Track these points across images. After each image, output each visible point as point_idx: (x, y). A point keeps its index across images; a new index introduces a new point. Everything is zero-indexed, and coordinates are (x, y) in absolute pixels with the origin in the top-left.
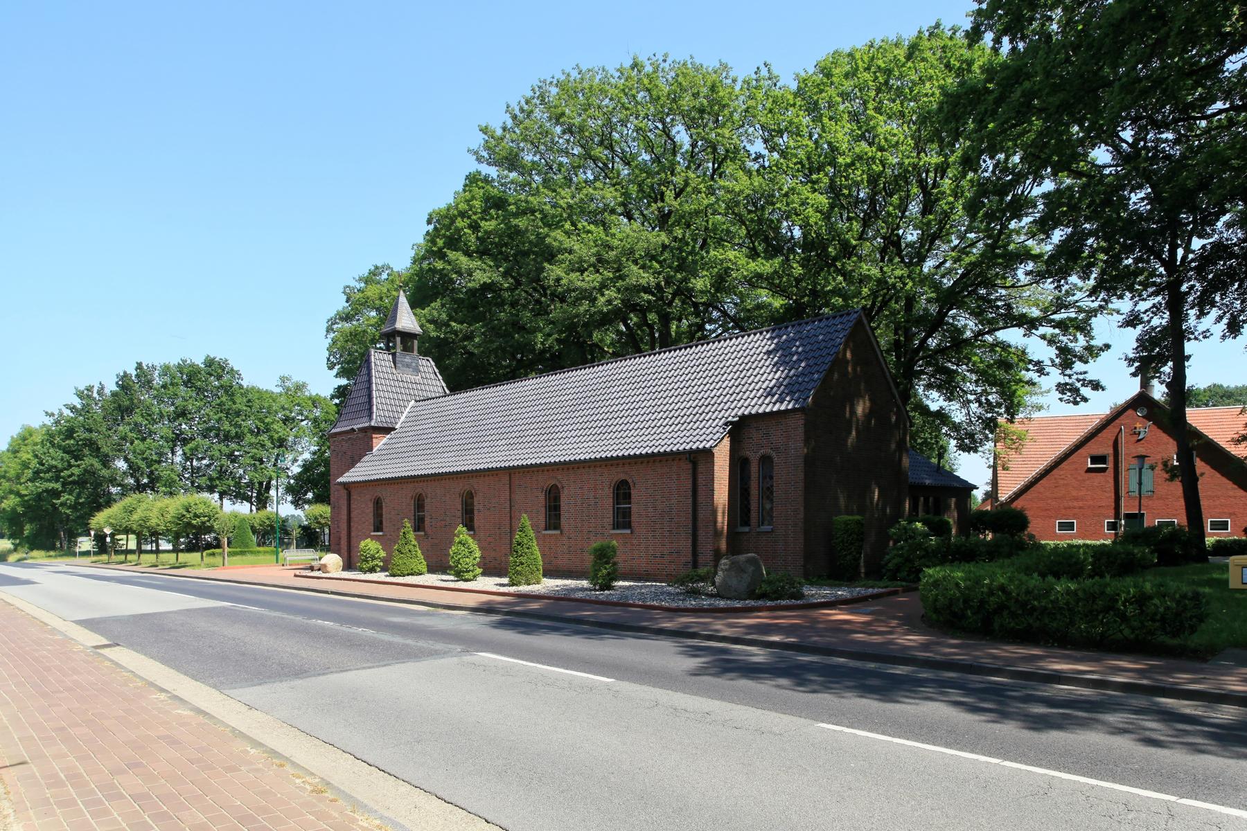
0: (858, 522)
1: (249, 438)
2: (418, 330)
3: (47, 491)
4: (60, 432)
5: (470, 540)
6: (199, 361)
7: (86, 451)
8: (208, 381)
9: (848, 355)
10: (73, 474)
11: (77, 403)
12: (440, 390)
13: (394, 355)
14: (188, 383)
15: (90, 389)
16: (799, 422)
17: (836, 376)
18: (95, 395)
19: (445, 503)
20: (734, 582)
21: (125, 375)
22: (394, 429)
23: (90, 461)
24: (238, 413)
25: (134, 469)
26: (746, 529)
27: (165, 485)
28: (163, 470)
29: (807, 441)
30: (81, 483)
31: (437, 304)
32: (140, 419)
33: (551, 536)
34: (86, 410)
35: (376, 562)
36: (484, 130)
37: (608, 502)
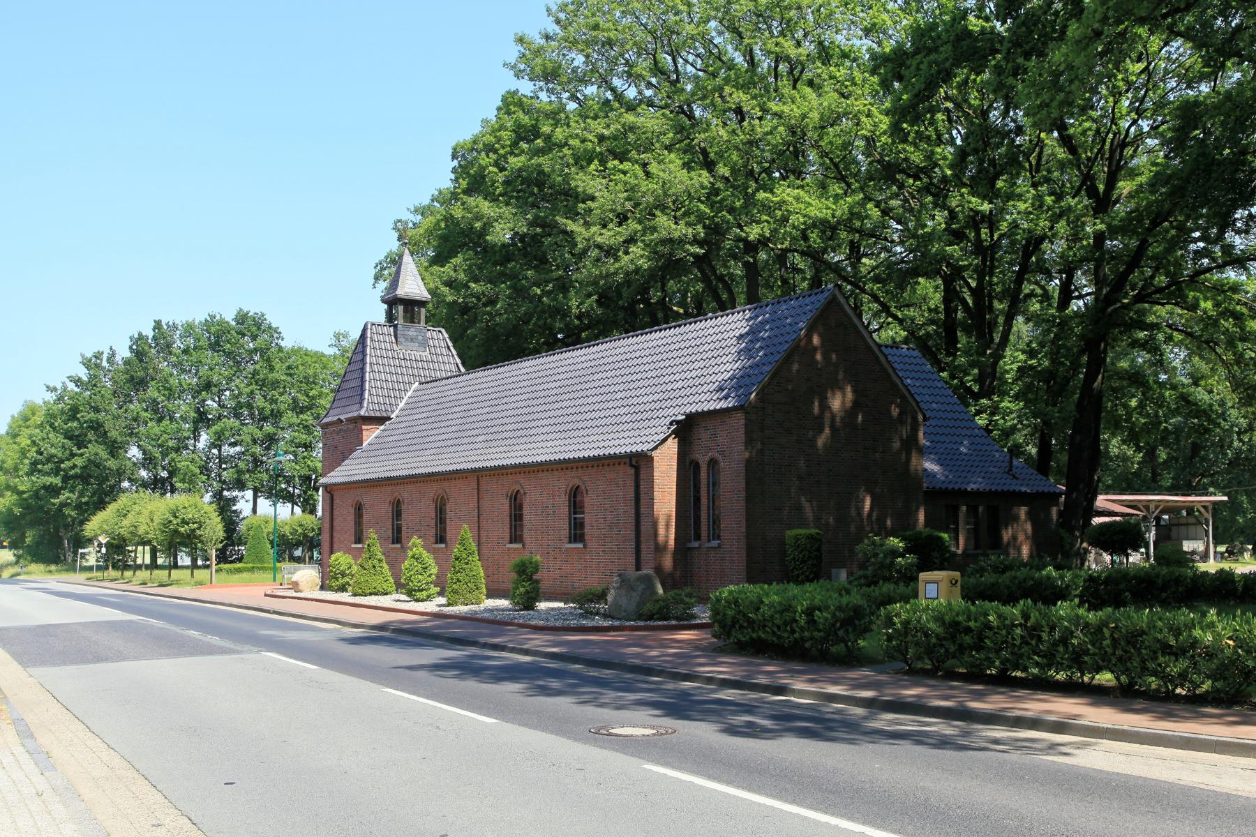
0: (811, 537)
1: (289, 417)
2: (424, 295)
3: (45, 487)
4: (62, 412)
5: (425, 554)
6: (229, 317)
7: (91, 435)
8: (240, 343)
9: (816, 340)
10: (75, 466)
11: (83, 374)
12: (453, 368)
13: (395, 327)
14: (215, 346)
15: (98, 356)
16: (739, 421)
17: (795, 367)
18: (105, 364)
19: (419, 509)
20: (623, 601)
21: (141, 337)
22: (389, 419)
23: (96, 450)
24: (275, 384)
25: (148, 461)
26: (696, 544)
27: (183, 481)
28: (183, 462)
29: (749, 442)
30: (84, 477)
31: (457, 260)
32: (156, 395)
33: (515, 549)
34: (93, 383)
35: (347, 579)
36: (521, 40)
37: (564, 511)
